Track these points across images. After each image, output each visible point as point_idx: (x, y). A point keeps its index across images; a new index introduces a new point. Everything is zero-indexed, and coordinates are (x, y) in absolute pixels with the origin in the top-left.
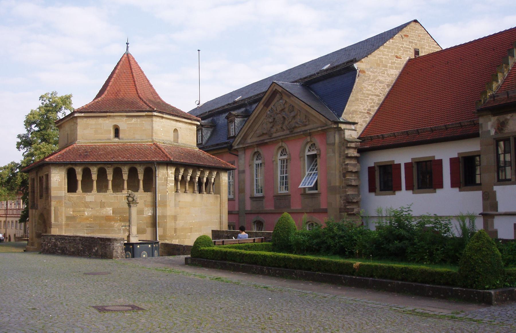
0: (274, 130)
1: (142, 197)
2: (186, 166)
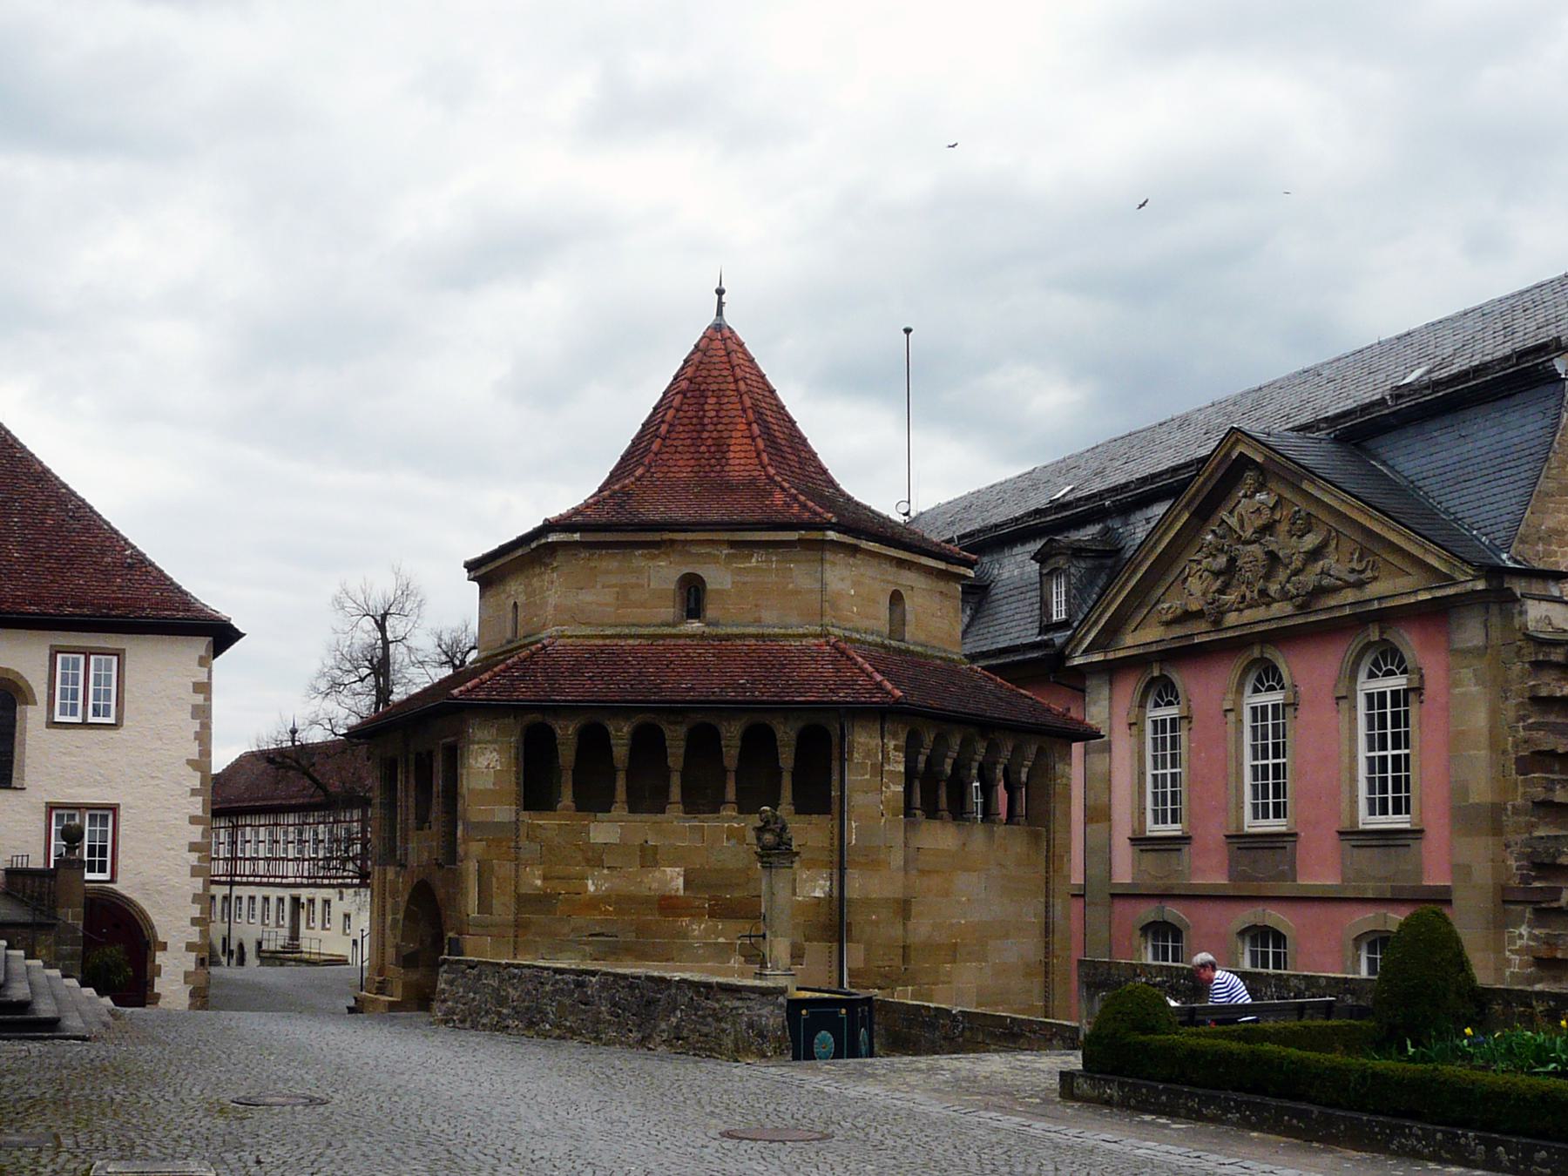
0: (1231, 597)
1: (807, 832)
2: (944, 719)
